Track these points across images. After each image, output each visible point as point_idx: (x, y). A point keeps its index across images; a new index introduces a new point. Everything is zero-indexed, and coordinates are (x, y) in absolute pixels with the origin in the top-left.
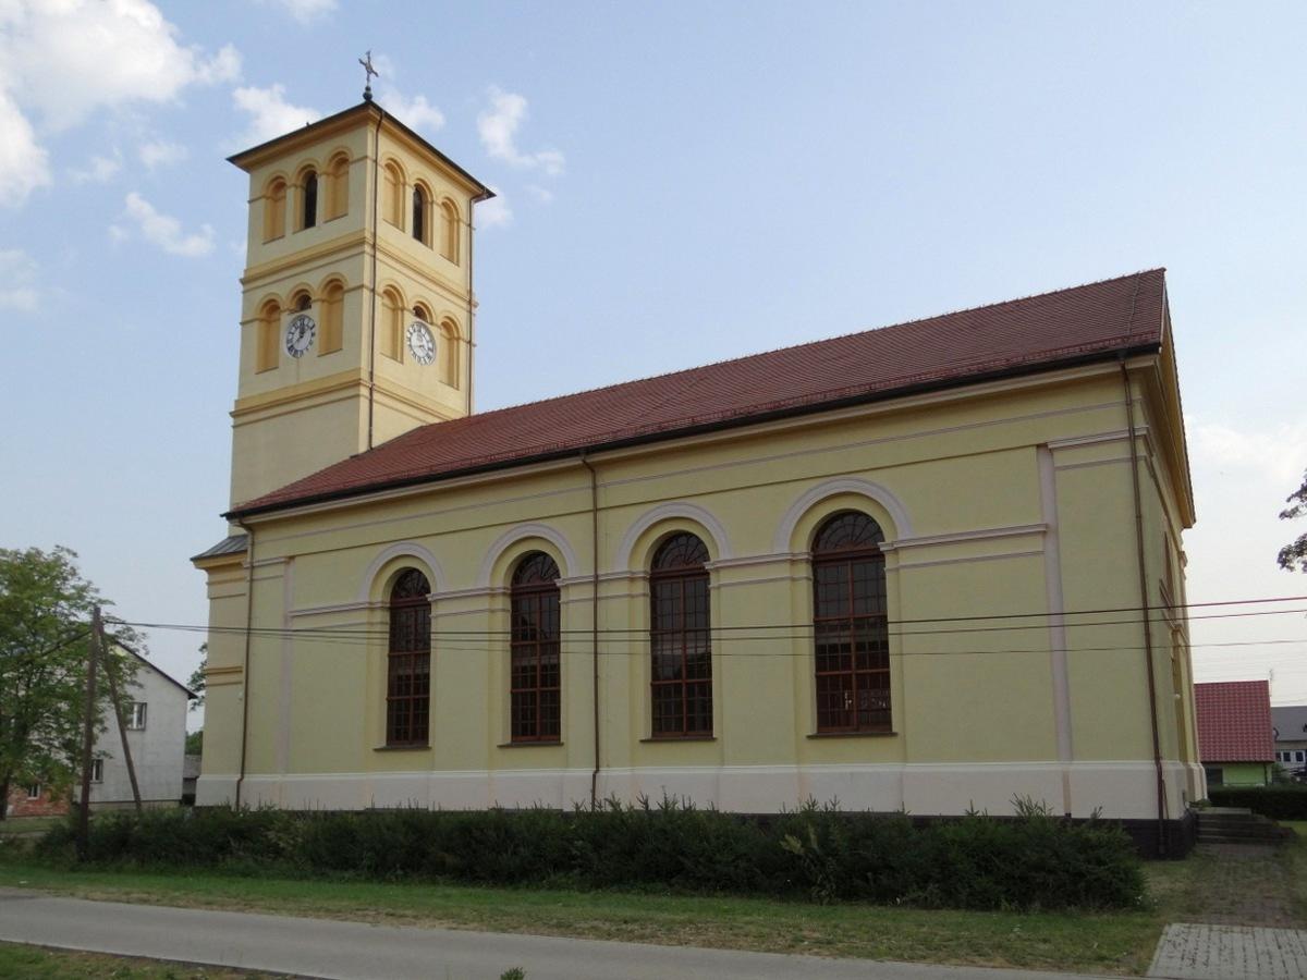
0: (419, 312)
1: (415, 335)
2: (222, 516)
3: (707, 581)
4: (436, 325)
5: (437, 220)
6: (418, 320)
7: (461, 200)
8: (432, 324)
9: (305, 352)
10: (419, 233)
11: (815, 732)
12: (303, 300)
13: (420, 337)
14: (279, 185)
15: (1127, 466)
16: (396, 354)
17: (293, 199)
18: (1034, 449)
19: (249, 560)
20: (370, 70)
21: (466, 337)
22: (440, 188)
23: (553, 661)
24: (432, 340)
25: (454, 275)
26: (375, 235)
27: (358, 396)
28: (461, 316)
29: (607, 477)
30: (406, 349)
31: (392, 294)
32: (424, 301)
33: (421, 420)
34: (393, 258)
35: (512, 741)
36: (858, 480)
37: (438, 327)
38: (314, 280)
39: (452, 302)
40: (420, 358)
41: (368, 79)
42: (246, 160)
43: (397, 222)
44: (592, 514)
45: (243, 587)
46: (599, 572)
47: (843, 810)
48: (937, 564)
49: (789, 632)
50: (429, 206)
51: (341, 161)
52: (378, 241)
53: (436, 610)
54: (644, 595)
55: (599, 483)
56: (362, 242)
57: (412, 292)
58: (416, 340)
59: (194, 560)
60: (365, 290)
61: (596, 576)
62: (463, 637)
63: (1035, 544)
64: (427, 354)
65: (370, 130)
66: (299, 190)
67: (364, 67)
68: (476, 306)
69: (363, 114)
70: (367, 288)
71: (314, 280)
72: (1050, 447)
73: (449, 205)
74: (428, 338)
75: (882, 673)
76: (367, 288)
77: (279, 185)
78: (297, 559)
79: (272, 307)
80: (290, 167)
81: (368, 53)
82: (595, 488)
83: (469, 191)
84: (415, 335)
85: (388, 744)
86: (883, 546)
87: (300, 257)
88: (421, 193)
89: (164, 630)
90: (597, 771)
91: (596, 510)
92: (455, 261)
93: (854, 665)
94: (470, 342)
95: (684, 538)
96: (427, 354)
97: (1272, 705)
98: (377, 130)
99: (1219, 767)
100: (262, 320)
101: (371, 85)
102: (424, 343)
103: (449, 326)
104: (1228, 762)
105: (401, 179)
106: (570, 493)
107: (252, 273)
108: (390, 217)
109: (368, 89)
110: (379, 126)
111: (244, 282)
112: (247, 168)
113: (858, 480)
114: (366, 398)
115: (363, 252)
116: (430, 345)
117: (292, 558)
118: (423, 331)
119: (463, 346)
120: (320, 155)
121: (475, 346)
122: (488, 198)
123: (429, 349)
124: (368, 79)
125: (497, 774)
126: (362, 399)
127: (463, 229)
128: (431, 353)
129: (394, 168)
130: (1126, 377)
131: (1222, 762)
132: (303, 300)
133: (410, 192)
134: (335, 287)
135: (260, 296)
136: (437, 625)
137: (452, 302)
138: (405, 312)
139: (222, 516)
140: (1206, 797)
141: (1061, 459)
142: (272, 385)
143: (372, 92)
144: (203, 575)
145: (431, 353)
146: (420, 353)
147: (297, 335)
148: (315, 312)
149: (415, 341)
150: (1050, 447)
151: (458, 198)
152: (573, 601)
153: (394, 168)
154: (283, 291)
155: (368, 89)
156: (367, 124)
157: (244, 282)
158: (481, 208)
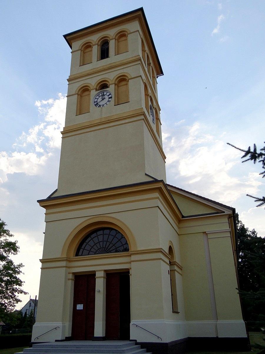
11: (68, 334)
12: (103, 86)
14: (88, 46)
17: (95, 51)
18: (202, 233)
38: (111, 77)
42: (70, 38)
54: (72, 279)
59: (38, 201)
66: (99, 47)
71: (111, 77)
72: (207, 233)
77: (88, 46)
79: (85, 90)
80: (95, 38)
89: (241, 149)
97: (71, 336)
107: (72, 77)
111: (68, 80)
120: (111, 33)
132: (103, 86)
135: (79, 84)
142: (83, 119)
144: (44, 210)
147: (100, 99)
150: (207, 233)
152: (133, 261)
154: (93, 82)
157: (68, 80)
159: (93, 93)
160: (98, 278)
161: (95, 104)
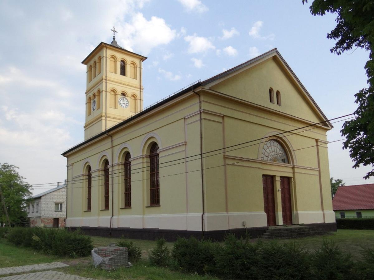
0: (124, 94)
2: (61, 155)
4: (129, 97)
7: (137, 61)
8: (127, 97)
10: (123, 72)
13: (124, 101)
16: (116, 107)
21: (140, 98)
24: (128, 101)
25: (136, 82)
26: (106, 76)
27: (102, 120)
28: (137, 93)
29: (115, 137)
30: (118, 105)
31: (113, 91)
32: (124, 91)
35: (105, 209)
38: (95, 91)
39: (134, 90)
41: (114, 34)
43: (115, 72)
46: (113, 164)
47: (248, 227)
48: (166, 156)
50: (126, 65)
51: (100, 58)
52: (107, 78)
55: (113, 140)
56: (102, 79)
57: (120, 89)
58: (121, 101)
60: (104, 92)
61: (112, 165)
62: (50, 185)
64: (126, 105)
65: (105, 49)
67: (112, 31)
68: (143, 89)
69: (101, 46)
70: (104, 91)
73: (133, 63)
74: (126, 100)
76: (104, 91)
78: (74, 164)
79: (90, 98)
81: (114, 27)
82: (112, 141)
83: (139, 58)
84: (122, 101)
85: (88, 210)
87: (123, 83)
88: (123, 61)
90: (203, 214)
91: (112, 147)
92: (136, 78)
94: (141, 100)
98: (106, 49)
99: (343, 212)
100: (89, 103)
101: (115, 36)
102: (125, 102)
103: (134, 96)
104: (363, 210)
105: (116, 60)
106: (107, 144)
108: (113, 70)
109: (114, 37)
110: (106, 47)
112: (86, 64)
114: (104, 120)
115: (103, 82)
116: (127, 102)
117: (73, 164)
118: (125, 99)
119: (139, 101)
121: (143, 100)
122: (146, 59)
123: (127, 103)
124: (114, 34)
125: (84, 218)
126: (103, 120)
127: (138, 69)
128: (127, 105)
129: (113, 57)
130: (198, 94)
131: (361, 210)
132: (94, 95)
134: (99, 92)
135: (88, 96)
137: (134, 90)
138: (118, 95)
139: (61, 155)
141: (189, 121)
143: (115, 37)
145: (127, 105)
149: (122, 102)
151: (136, 61)
153: (113, 57)
155: (114, 37)
156: (103, 48)
158: (143, 63)
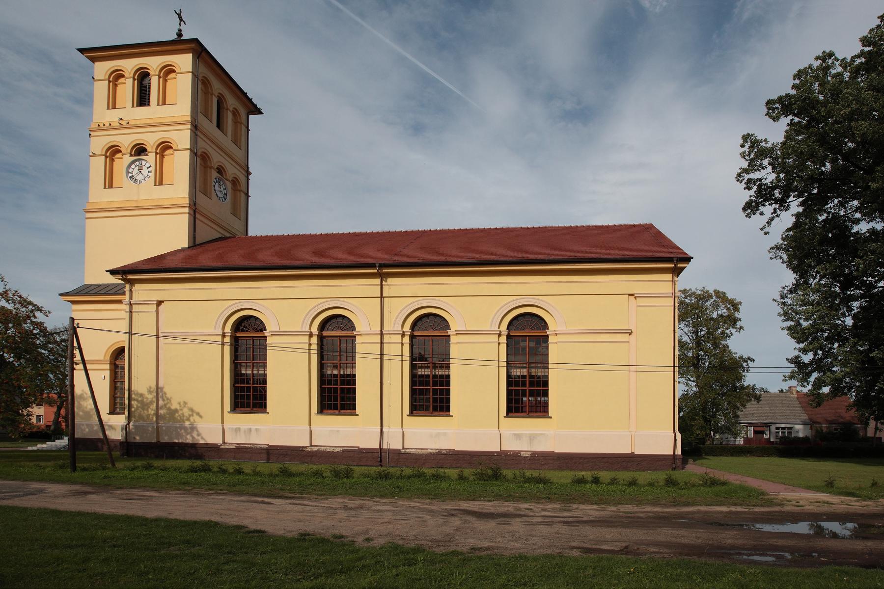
1: (217, 184)
2: (107, 271)
3: (266, 341)
5: (229, 118)
6: (219, 176)
7: (243, 112)
9: (143, 181)
12: (140, 150)
15: (672, 308)
17: (127, 89)
19: (127, 299)
20: (181, 19)
22: (231, 102)
23: (546, 374)
30: (213, 191)
33: (222, 234)
34: (203, 134)
36: (255, 303)
37: (230, 182)
40: (219, 198)
41: (180, 24)
44: (384, 296)
45: (126, 315)
49: (627, 368)
53: (359, 340)
63: (625, 337)
71: (151, 140)
73: (235, 113)
75: (353, 388)
80: (129, 65)
84: (217, 184)
86: (266, 333)
93: (528, 385)
95: (341, 318)
96: (224, 197)
109: (180, 30)
113: (255, 303)
124: (180, 24)
133: (215, 100)
136: (359, 348)
139: (107, 271)
140: (679, 452)
146: (221, 195)
148: (150, 159)
149: (217, 188)
154: (126, 141)
155: (180, 30)
159: (128, 159)
160: (452, 343)
161: (130, 175)
